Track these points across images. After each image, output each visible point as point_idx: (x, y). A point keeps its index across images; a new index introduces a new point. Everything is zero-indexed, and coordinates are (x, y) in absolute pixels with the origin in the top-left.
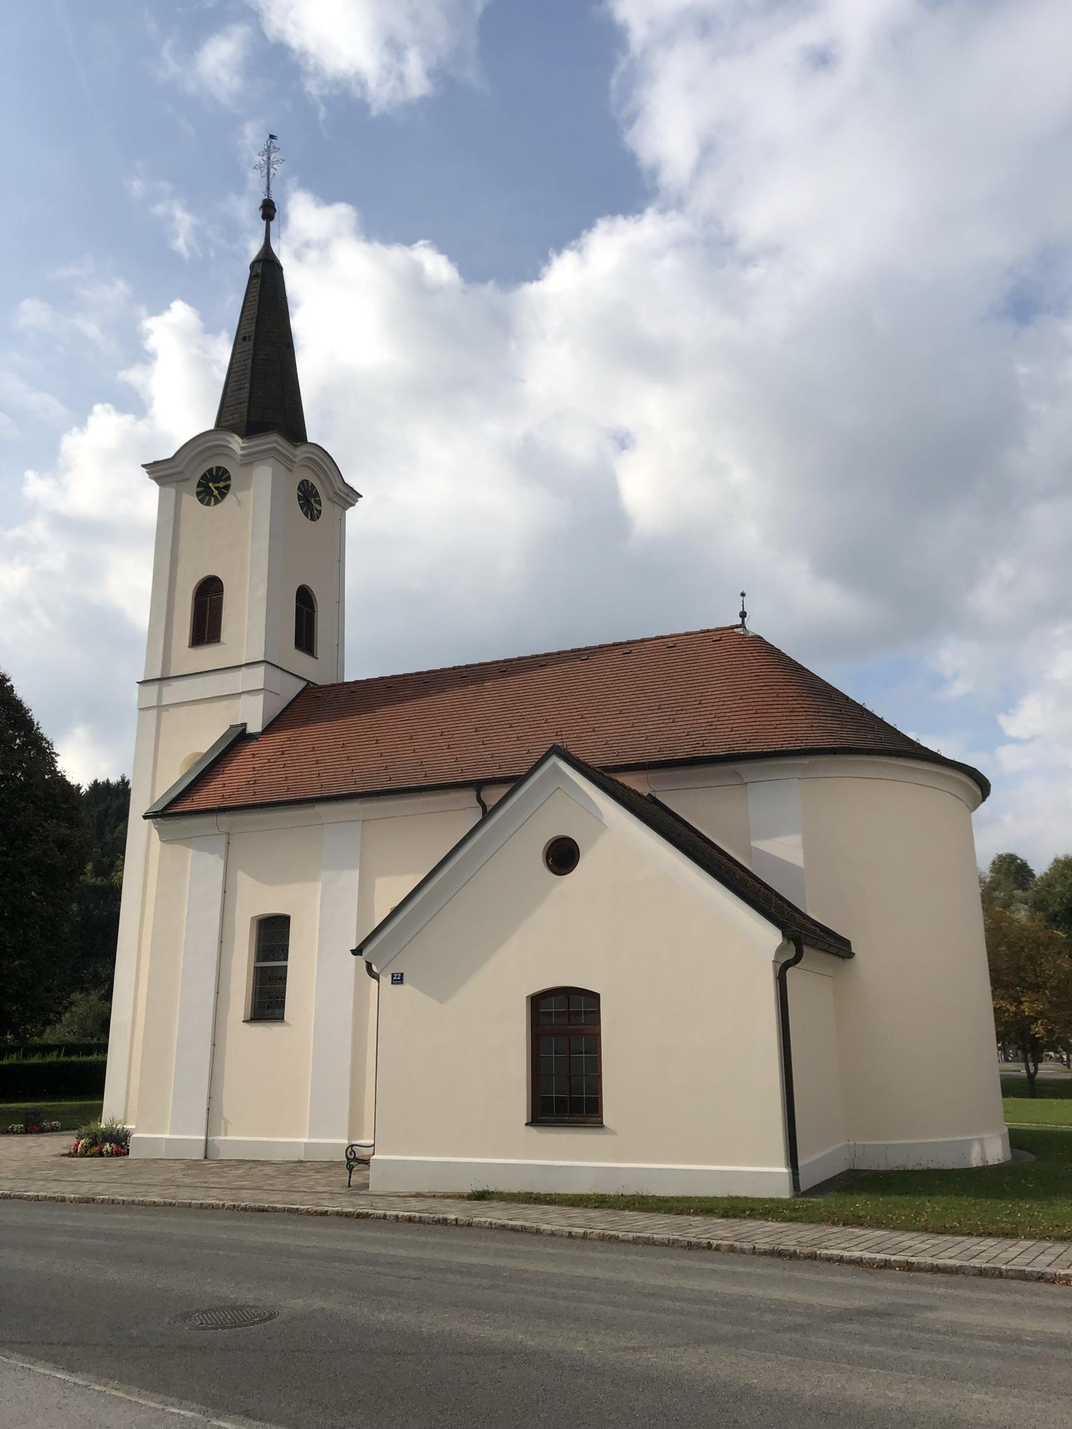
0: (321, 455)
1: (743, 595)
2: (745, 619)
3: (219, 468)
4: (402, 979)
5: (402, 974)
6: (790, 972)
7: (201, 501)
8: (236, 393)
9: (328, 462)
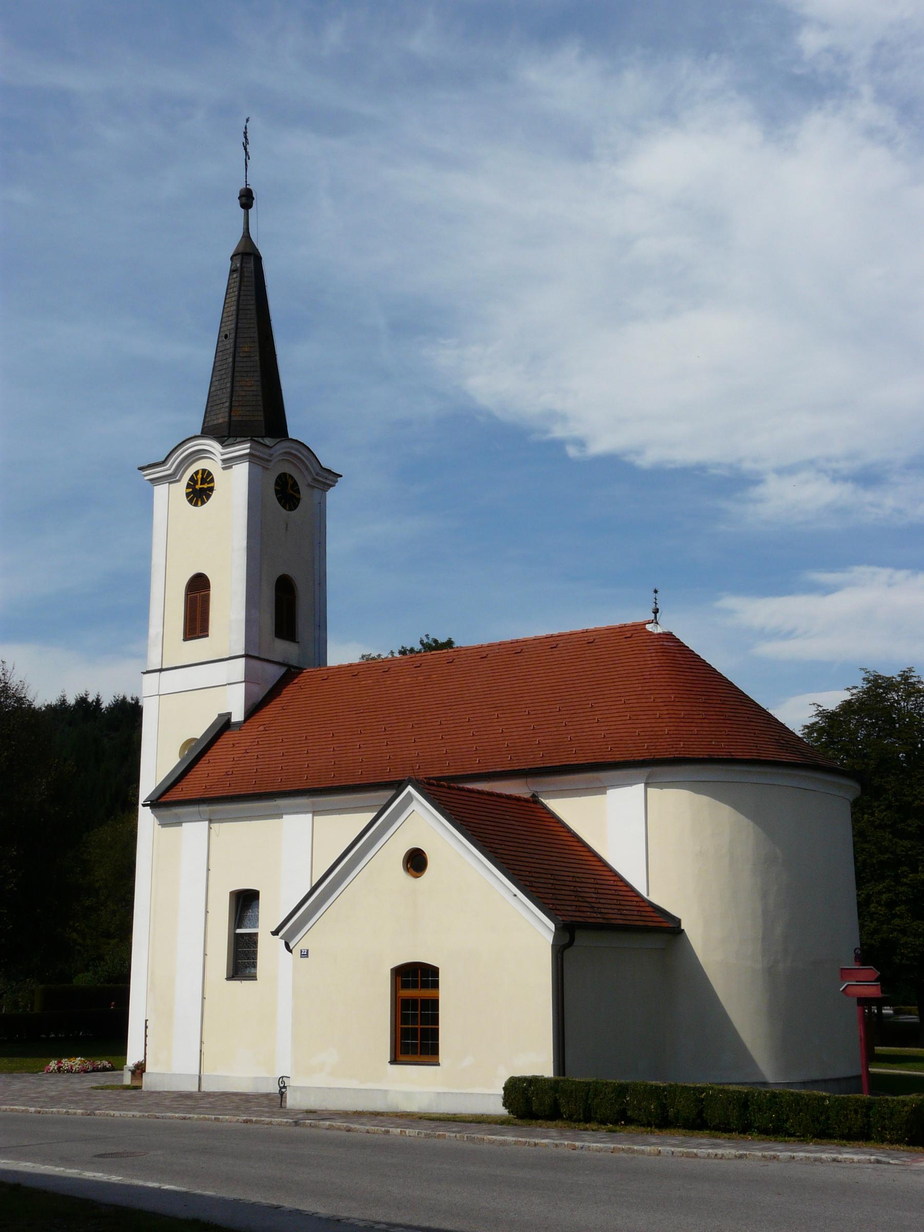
0: (297, 447)
1: (656, 592)
2: (657, 614)
3: (204, 471)
4: (307, 954)
5: (308, 950)
6: (567, 953)
7: (190, 501)
8: (219, 393)
9: (305, 453)
